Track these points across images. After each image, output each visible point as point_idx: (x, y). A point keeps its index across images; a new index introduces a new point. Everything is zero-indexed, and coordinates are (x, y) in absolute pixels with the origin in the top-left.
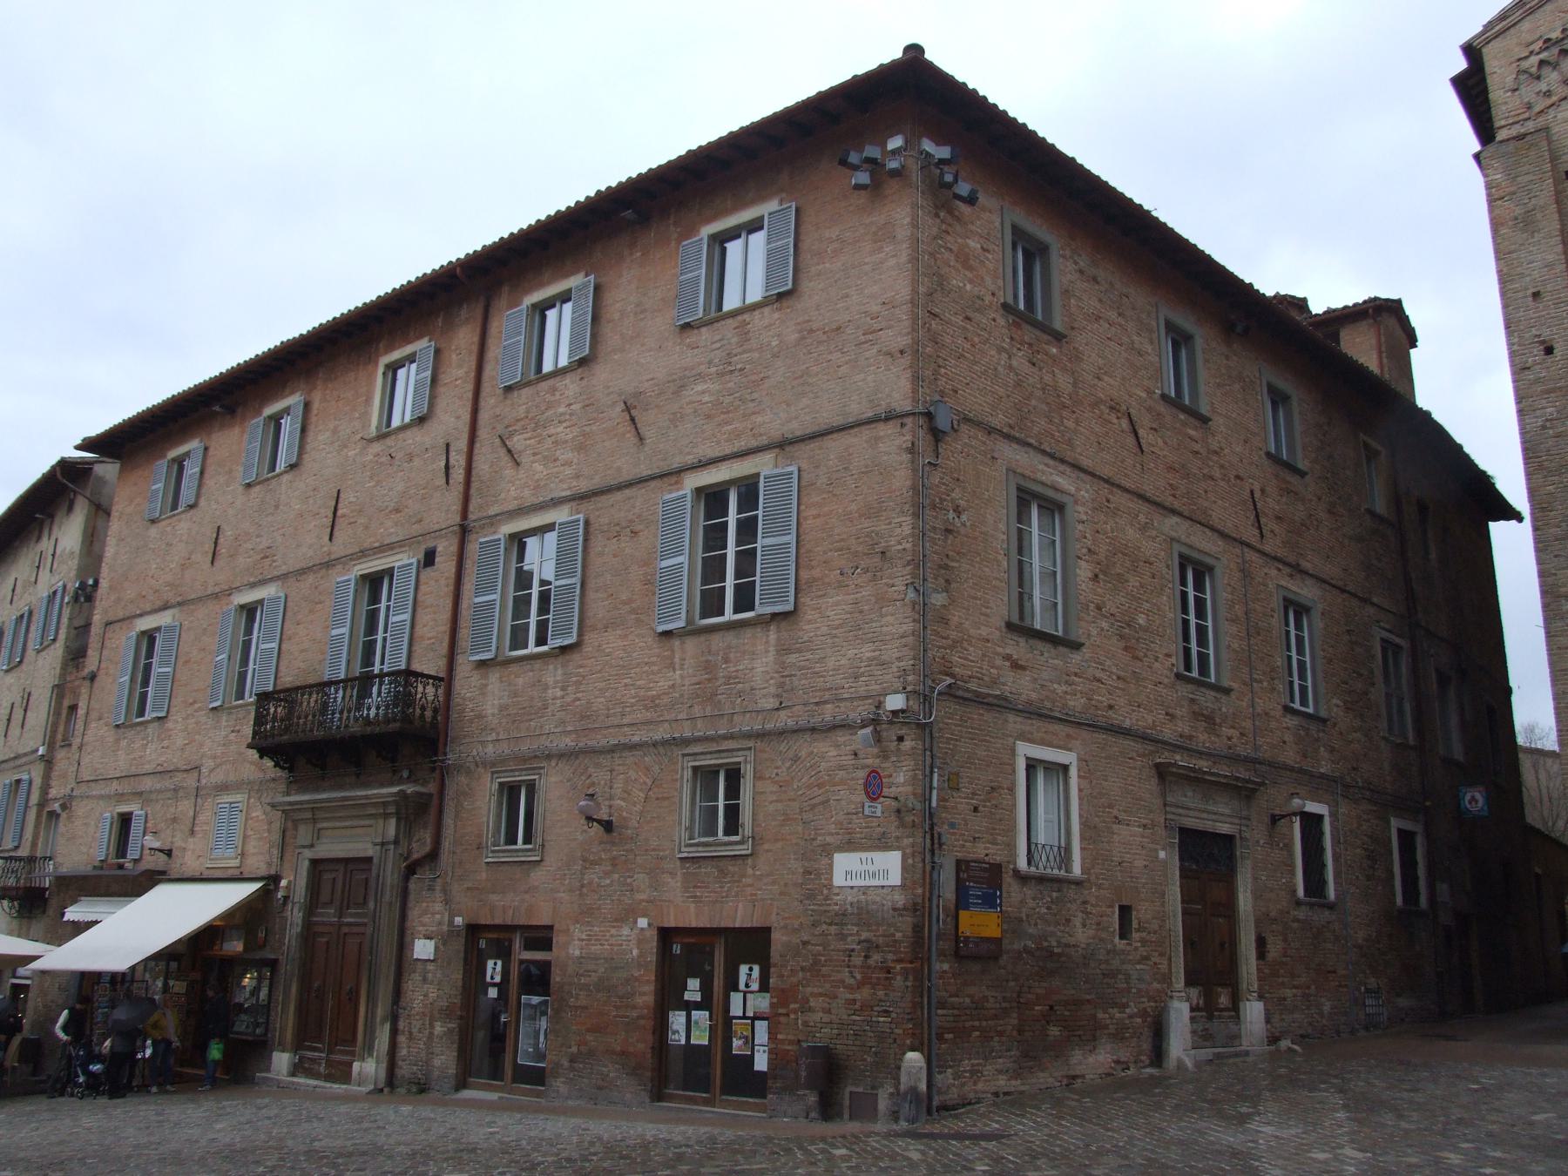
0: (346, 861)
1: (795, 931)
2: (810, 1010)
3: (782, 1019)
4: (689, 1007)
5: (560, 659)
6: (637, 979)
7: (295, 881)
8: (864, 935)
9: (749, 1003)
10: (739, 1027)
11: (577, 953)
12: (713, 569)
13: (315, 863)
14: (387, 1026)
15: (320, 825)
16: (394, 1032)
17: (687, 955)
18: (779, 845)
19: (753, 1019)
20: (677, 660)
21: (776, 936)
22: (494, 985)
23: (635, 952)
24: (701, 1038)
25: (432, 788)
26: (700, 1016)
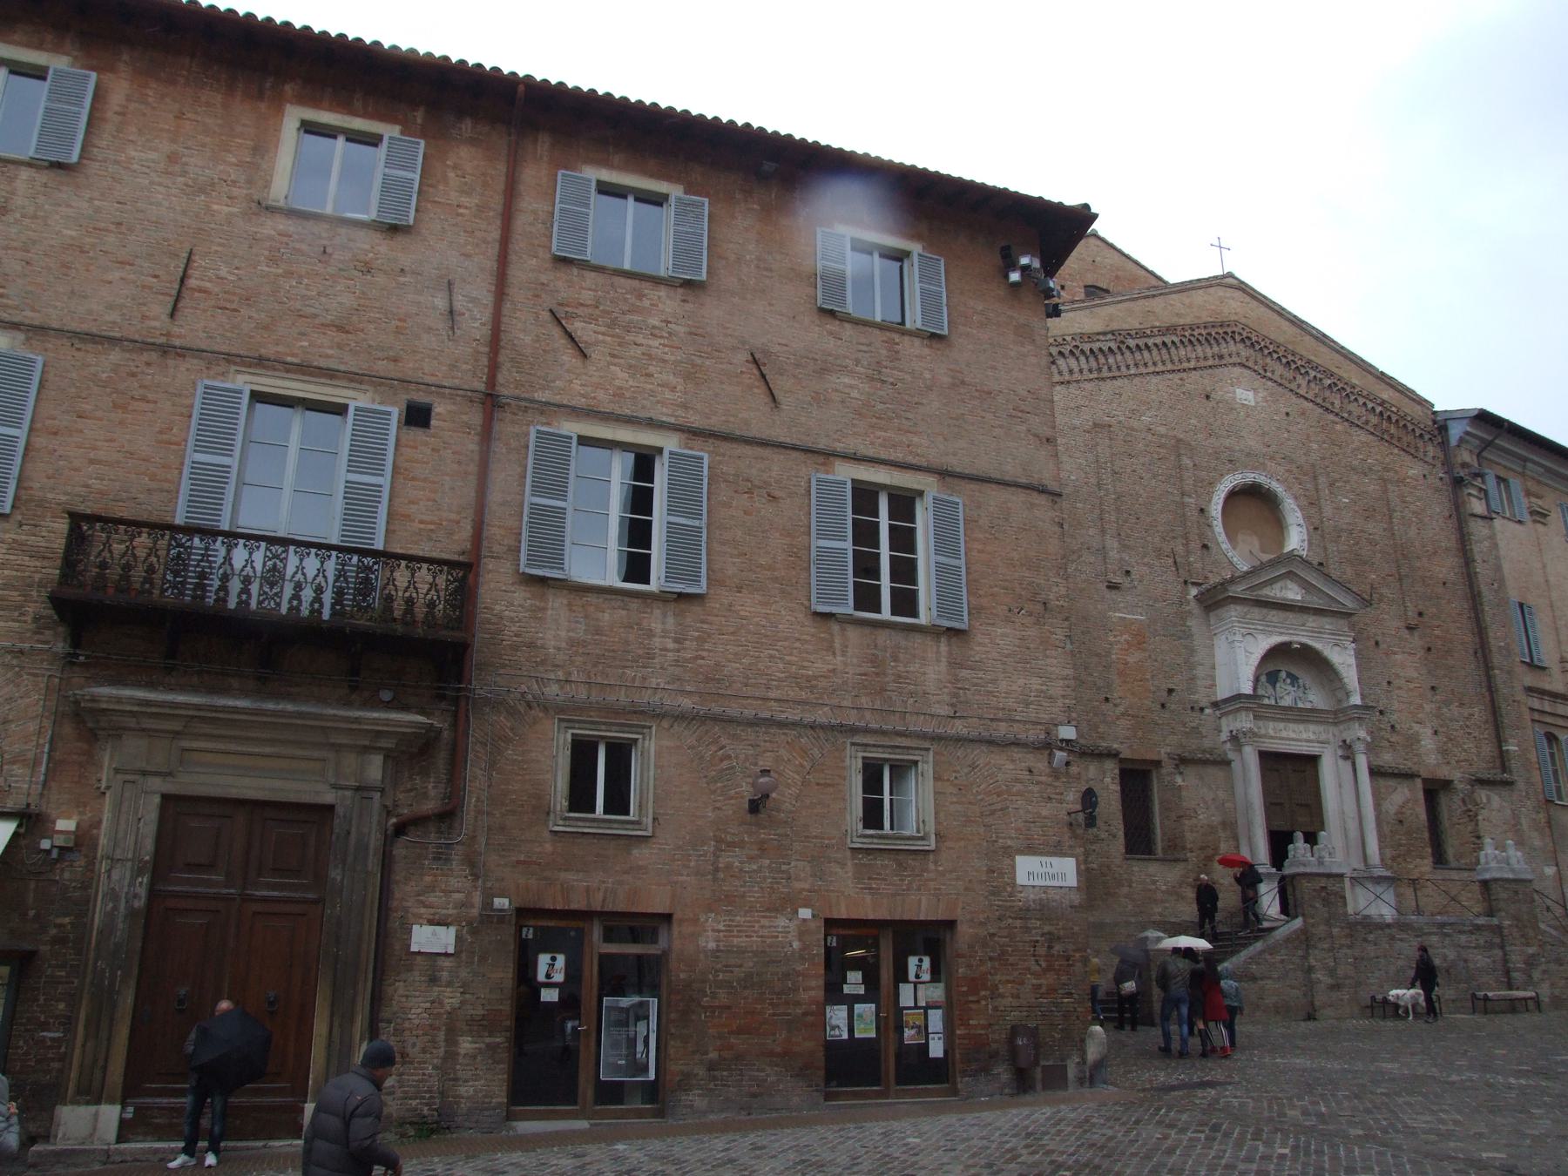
1: (981, 924)
2: (1002, 996)
3: (973, 1006)
4: (852, 1000)
5: (672, 605)
6: (798, 974)
8: (1047, 929)
9: (920, 994)
10: (911, 1017)
11: (712, 945)
12: (866, 566)
17: (866, 948)
18: (962, 843)
19: (926, 1009)
20: (837, 645)
21: (965, 931)
23: (796, 945)
24: (865, 1031)
26: (866, 1010)
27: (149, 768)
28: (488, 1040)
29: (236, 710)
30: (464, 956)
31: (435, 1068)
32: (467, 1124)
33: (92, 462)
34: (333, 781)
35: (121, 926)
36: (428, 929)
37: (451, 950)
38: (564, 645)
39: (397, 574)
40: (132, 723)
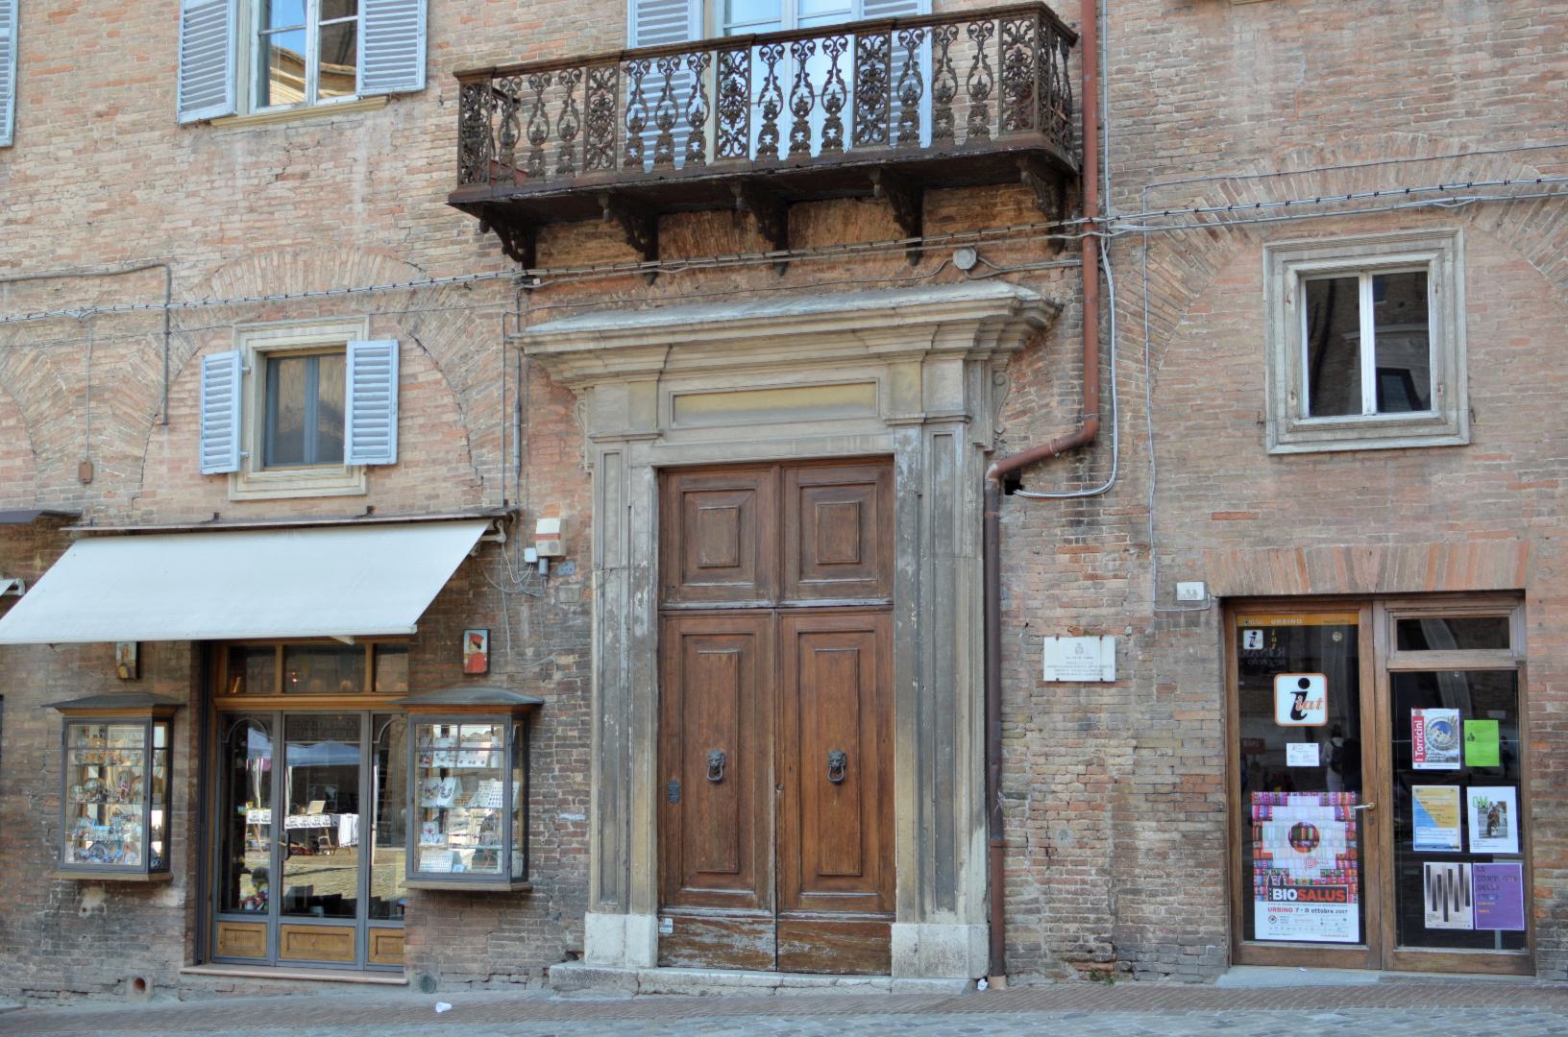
7: (599, 520)
13: (662, 472)
14: (980, 836)
16: (998, 850)
22: (1310, 734)
25: (1057, 287)
27: (633, 431)
28: (1184, 827)
29: (719, 326)
30: (1133, 685)
31: (1102, 871)
32: (1161, 967)
34: (885, 413)
35: (624, 664)
36: (1069, 643)
37: (1109, 675)
38: (1268, 108)
39: (954, 50)
40: (596, 367)
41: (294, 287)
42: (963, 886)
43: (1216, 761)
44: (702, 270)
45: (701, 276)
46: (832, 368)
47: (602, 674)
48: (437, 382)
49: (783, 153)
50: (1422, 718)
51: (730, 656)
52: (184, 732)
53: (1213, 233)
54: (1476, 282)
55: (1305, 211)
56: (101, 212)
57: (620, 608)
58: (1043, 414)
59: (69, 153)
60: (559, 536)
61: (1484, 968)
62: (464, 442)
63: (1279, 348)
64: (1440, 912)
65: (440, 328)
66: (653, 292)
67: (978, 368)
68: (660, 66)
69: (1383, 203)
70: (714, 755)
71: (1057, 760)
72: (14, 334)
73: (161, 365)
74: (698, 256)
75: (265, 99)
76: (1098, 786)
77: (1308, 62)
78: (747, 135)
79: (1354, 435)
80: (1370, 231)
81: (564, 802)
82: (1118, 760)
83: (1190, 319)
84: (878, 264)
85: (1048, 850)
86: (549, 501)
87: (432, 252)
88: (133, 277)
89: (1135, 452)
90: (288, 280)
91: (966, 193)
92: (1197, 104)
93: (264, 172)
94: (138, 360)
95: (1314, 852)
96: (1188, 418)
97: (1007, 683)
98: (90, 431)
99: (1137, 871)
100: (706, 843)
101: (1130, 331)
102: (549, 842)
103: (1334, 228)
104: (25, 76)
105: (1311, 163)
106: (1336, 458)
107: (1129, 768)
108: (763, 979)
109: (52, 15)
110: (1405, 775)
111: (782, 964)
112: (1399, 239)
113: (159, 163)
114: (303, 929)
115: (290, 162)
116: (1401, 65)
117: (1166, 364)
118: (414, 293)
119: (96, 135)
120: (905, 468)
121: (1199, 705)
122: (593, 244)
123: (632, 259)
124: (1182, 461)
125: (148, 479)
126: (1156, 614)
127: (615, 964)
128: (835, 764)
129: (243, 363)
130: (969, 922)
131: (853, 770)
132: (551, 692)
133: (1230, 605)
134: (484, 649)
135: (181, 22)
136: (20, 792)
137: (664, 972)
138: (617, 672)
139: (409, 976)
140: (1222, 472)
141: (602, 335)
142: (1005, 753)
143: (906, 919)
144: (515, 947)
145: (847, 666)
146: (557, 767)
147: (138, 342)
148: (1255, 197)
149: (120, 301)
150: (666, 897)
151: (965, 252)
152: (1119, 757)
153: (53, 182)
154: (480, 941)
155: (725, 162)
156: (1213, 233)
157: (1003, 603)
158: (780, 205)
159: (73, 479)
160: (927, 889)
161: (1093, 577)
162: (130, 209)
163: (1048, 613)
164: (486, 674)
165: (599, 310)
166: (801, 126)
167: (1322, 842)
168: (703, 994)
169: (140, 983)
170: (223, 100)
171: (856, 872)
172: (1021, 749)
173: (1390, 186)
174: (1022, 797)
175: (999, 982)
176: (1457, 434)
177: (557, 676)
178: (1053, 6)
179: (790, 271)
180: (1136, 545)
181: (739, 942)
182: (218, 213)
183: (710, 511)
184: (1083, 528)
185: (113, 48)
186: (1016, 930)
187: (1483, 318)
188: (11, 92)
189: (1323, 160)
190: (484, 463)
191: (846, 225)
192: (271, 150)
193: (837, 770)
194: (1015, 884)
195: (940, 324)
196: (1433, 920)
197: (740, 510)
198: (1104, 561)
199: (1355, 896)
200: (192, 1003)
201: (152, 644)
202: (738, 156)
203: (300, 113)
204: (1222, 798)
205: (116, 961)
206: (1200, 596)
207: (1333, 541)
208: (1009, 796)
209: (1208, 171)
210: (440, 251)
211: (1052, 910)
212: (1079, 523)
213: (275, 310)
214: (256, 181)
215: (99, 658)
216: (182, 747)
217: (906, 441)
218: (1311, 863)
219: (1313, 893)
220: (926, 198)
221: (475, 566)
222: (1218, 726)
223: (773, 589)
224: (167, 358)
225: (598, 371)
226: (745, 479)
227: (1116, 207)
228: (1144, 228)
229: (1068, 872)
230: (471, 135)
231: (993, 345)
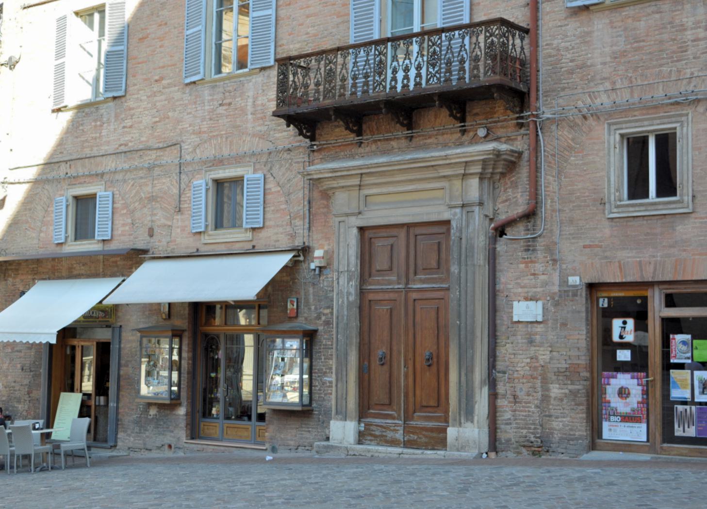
0: (409, 226)
7: (337, 249)
13: (362, 229)
14: (485, 390)
15: (366, 192)
16: (493, 396)
25: (520, 144)
27: (349, 212)
28: (570, 387)
29: (378, 165)
30: (550, 323)
31: (537, 407)
32: (560, 450)
33: (308, 17)
37: (540, 319)
38: (608, 59)
40: (334, 184)
41: (226, 152)
42: (476, 412)
43: (583, 358)
44: (379, 140)
45: (379, 143)
46: (425, 183)
47: (337, 318)
48: (279, 192)
49: (399, 89)
50: (674, 339)
51: (387, 309)
52: (185, 342)
53: (585, 117)
54: (697, 136)
55: (623, 106)
56: (156, 122)
57: (343, 288)
58: (513, 201)
59: (145, 97)
60: (323, 258)
61: (699, 455)
62: (289, 217)
63: (612, 169)
64: (681, 428)
65: (280, 168)
66: (361, 150)
67: (486, 182)
68: (364, 51)
69: (657, 101)
70: (380, 353)
71: (519, 357)
72: (125, 175)
73: (178, 187)
74: (378, 134)
75: (219, 71)
76: (535, 368)
77: (625, 37)
78: (385, 82)
79: (642, 208)
80: (652, 114)
81: (325, 373)
82: (543, 357)
83: (575, 156)
84: (449, 136)
85: (515, 397)
86: (320, 242)
87: (278, 135)
88: (168, 149)
89: (552, 218)
90: (224, 149)
91: (483, 102)
92: (579, 58)
93: (215, 103)
94: (169, 184)
95: (628, 400)
96: (574, 202)
97: (498, 322)
98: (153, 215)
99: (551, 407)
100: (379, 393)
101: (550, 163)
102: (320, 390)
103: (636, 113)
104: (130, 66)
105: (626, 83)
106: (636, 219)
107: (548, 361)
108: (396, 450)
109: (140, 39)
110: (668, 366)
111: (408, 444)
112: (663, 117)
113: (178, 100)
114: (232, 426)
115: (225, 98)
116: (665, 36)
117: (565, 178)
118: (270, 153)
119: (155, 89)
120: (455, 226)
121: (577, 332)
122: (337, 130)
123: (352, 137)
124: (571, 221)
125: (173, 234)
126: (559, 291)
127: (341, 443)
128: (427, 357)
129: (67, 201)
130: (479, 428)
131: (435, 360)
132: (321, 325)
133: (592, 287)
134: (295, 307)
135: (185, 40)
136: (127, 366)
137: (361, 446)
138: (343, 316)
139: (267, 446)
140: (587, 226)
141: (334, 171)
142: (498, 354)
143: (453, 426)
144: (307, 435)
145: (433, 314)
146: (323, 357)
147: (170, 177)
148: (604, 100)
149: (163, 160)
150: (363, 413)
151: (482, 129)
152: (544, 355)
153: (139, 110)
154: (294, 432)
155: (377, 94)
156: (585, 117)
157: (497, 286)
158: (407, 112)
159: (146, 235)
160: (462, 412)
161: (534, 274)
162: (167, 121)
163: (515, 291)
164: (297, 317)
165: (340, 159)
166: (406, 77)
167: (632, 395)
168: (372, 456)
169: (170, 446)
170: (199, 73)
171: (436, 405)
172: (504, 351)
173: (659, 93)
174: (504, 373)
175: (493, 455)
176: (688, 207)
177: (323, 318)
178: (506, 17)
179: (414, 140)
180: (551, 260)
181: (390, 435)
182: (198, 121)
183: (380, 245)
184: (530, 252)
185: (161, 52)
186: (501, 432)
187: (699, 153)
188: (124, 73)
189: (631, 82)
190: (296, 226)
191: (436, 118)
192: (218, 93)
193: (428, 360)
194: (501, 412)
195: (466, 162)
196: (678, 432)
197: (392, 246)
198: (539, 267)
199: (645, 420)
200: (188, 455)
201: (174, 304)
202: (382, 91)
203: (230, 77)
204: (587, 374)
205: (161, 437)
206: (578, 283)
207: (634, 257)
208: (499, 372)
209: (583, 88)
210: (280, 135)
211: (517, 423)
212: (528, 250)
213: (219, 162)
214: (212, 107)
215: (155, 310)
216: (185, 348)
217: (455, 214)
218: (627, 404)
219: (627, 418)
220: (468, 105)
221: (289, 270)
222: (585, 342)
223: (404, 280)
224: (180, 183)
225: (335, 186)
226: (394, 232)
227: (545, 108)
228: (556, 116)
229: (523, 407)
230: (282, 86)
231: (490, 170)
